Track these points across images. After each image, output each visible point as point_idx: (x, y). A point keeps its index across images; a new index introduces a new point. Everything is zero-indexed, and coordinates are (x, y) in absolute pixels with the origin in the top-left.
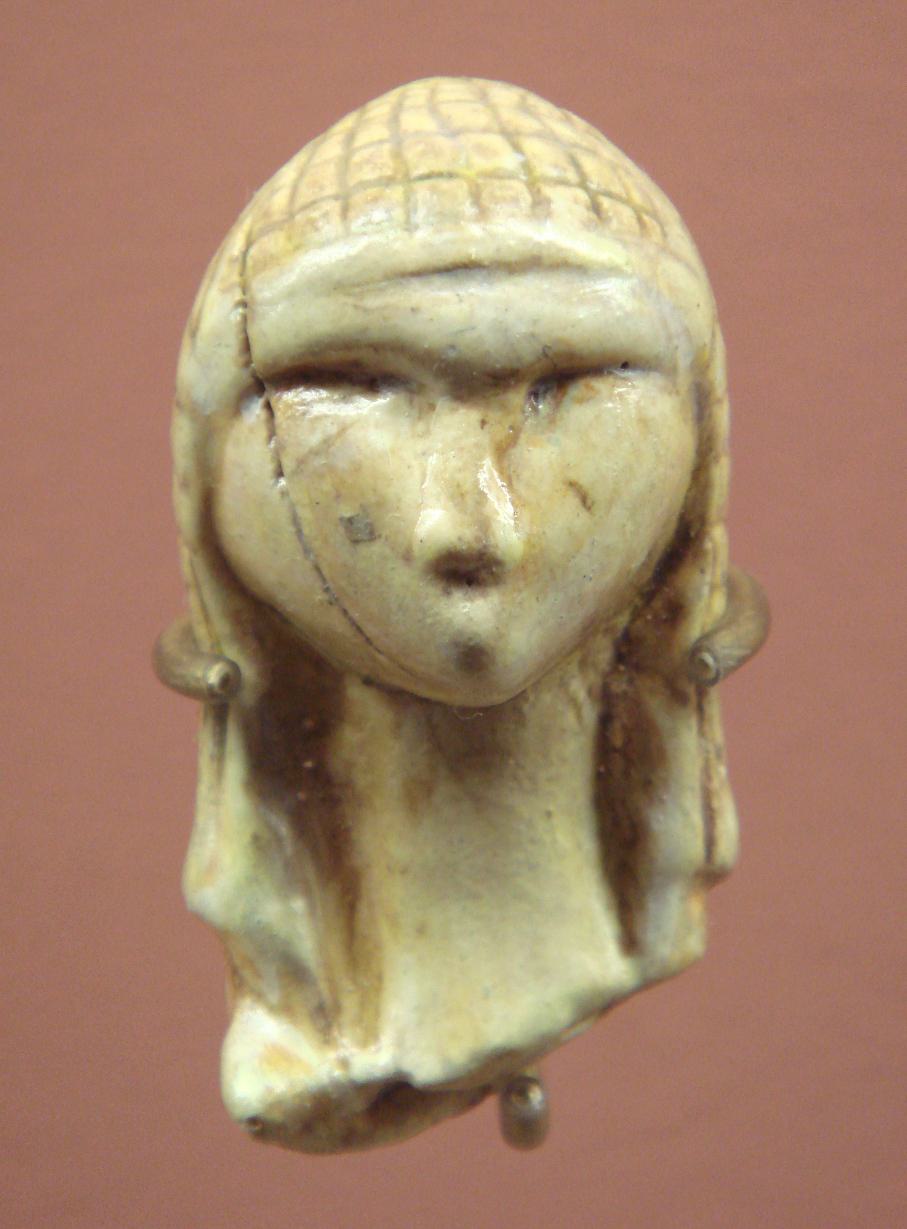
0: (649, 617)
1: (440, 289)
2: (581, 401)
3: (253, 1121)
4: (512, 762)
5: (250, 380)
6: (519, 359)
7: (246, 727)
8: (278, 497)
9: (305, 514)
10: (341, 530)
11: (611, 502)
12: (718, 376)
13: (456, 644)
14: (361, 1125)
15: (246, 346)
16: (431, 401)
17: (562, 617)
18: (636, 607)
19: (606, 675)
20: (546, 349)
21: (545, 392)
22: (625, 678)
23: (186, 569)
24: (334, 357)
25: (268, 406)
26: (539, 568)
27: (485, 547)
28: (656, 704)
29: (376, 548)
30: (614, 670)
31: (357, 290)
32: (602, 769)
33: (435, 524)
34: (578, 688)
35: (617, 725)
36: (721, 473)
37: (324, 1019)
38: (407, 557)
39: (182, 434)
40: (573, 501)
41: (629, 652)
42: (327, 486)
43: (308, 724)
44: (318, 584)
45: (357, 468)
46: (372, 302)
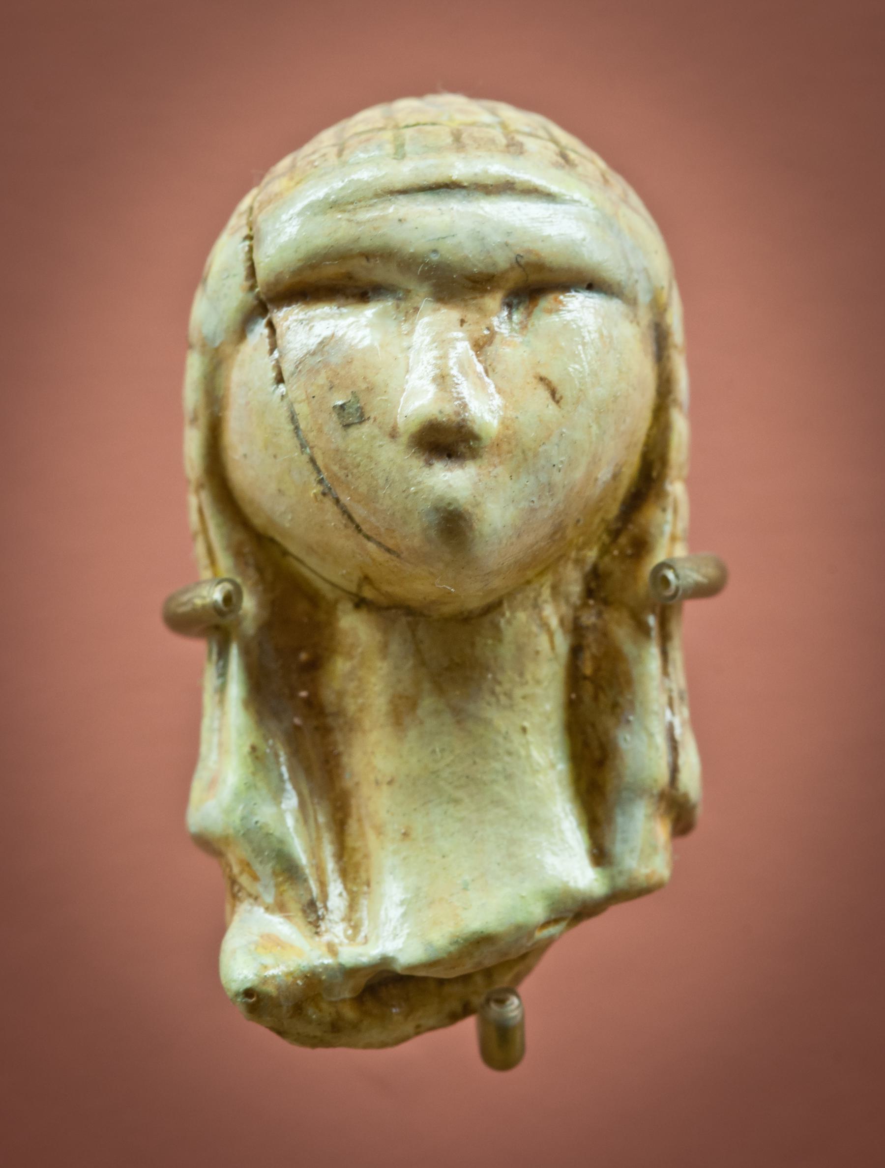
0: (616, 552)
1: (424, 205)
2: (550, 311)
3: (249, 993)
4: (490, 676)
5: (255, 302)
6: (494, 264)
7: (246, 652)
8: (279, 400)
9: (302, 409)
10: (334, 417)
11: (577, 402)
12: (675, 319)
13: (437, 509)
14: (350, 1013)
15: (252, 272)
16: (415, 305)
17: (533, 501)
18: (604, 544)
19: (576, 609)
20: (519, 259)
21: (519, 304)
22: (593, 611)
23: (194, 517)
24: (331, 270)
25: (271, 325)
26: (513, 449)
27: (463, 420)
28: (622, 634)
29: (366, 429)
30: (585, 605)
31: (351, 207)
32: (573, 696)
33: (417, 400)
34: (551, 613)
35: (587, 655)
36: (680, 426)
37: (313, 913)
38: (393, 435)
39: (194, 367)
40: (543, 394)
41: (596, 586)
42: (322, 379)
43: (304, 656)
44: (313, 478)
45: (349, 362)
46: (365, 215)
